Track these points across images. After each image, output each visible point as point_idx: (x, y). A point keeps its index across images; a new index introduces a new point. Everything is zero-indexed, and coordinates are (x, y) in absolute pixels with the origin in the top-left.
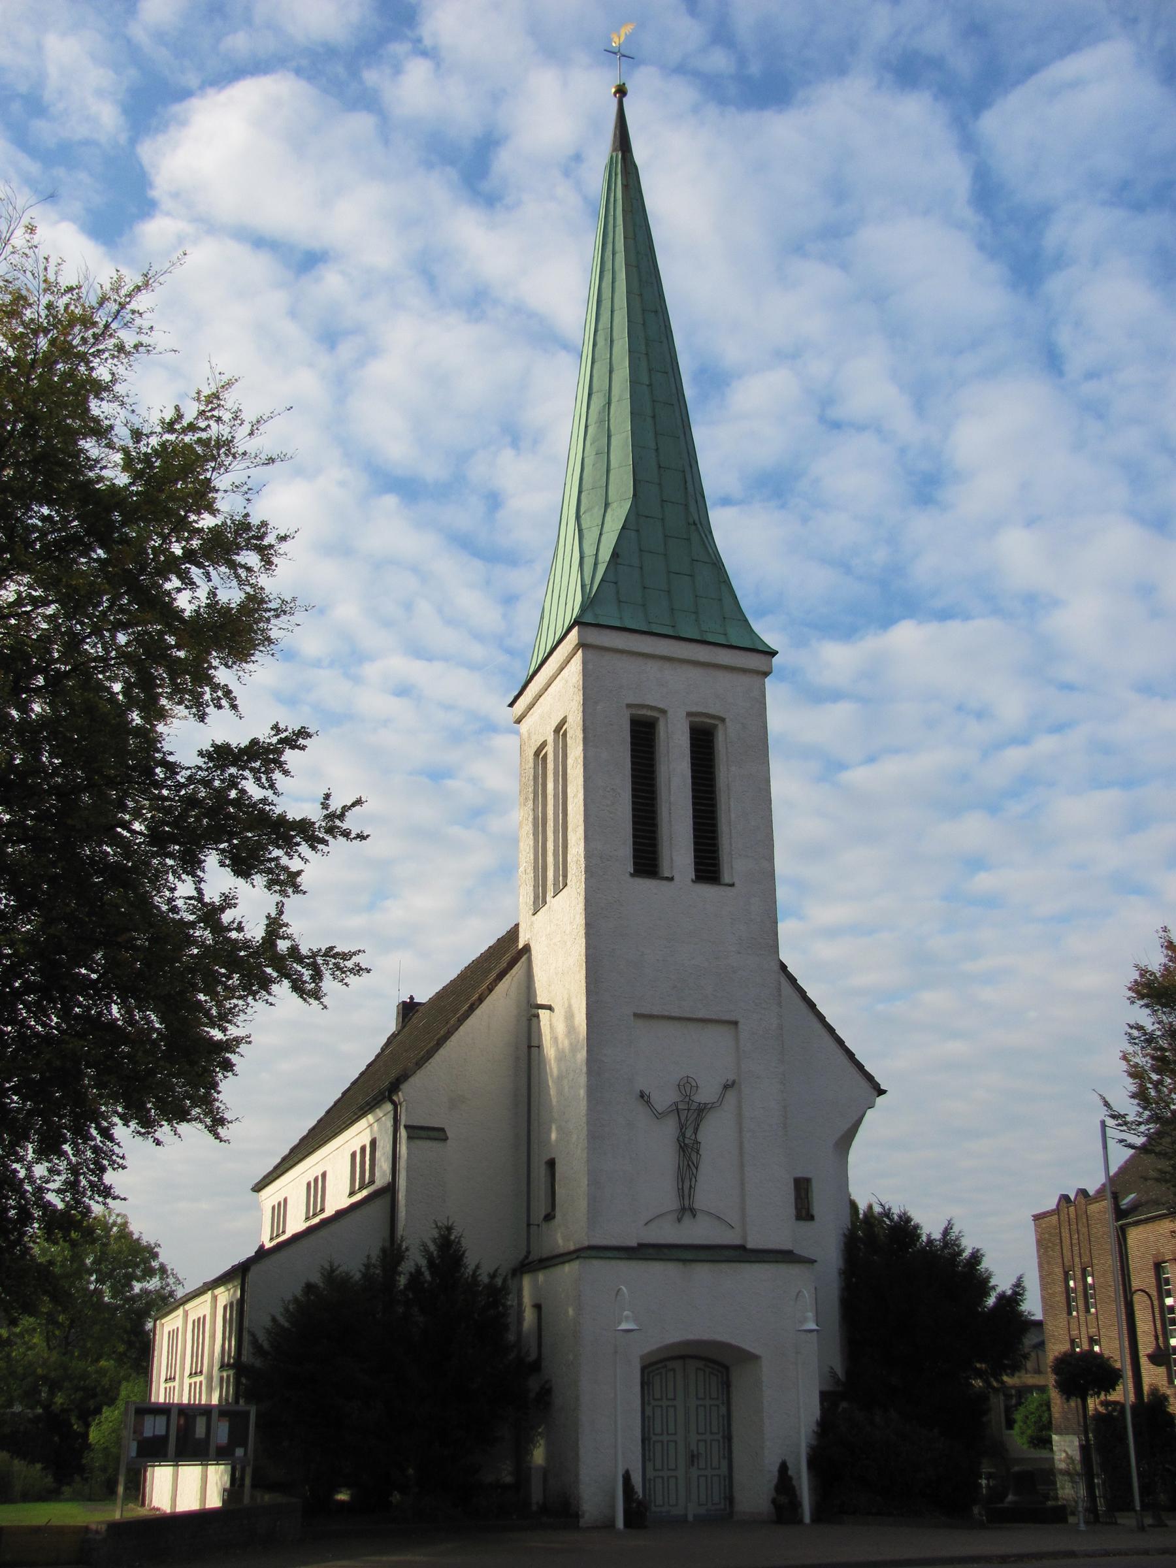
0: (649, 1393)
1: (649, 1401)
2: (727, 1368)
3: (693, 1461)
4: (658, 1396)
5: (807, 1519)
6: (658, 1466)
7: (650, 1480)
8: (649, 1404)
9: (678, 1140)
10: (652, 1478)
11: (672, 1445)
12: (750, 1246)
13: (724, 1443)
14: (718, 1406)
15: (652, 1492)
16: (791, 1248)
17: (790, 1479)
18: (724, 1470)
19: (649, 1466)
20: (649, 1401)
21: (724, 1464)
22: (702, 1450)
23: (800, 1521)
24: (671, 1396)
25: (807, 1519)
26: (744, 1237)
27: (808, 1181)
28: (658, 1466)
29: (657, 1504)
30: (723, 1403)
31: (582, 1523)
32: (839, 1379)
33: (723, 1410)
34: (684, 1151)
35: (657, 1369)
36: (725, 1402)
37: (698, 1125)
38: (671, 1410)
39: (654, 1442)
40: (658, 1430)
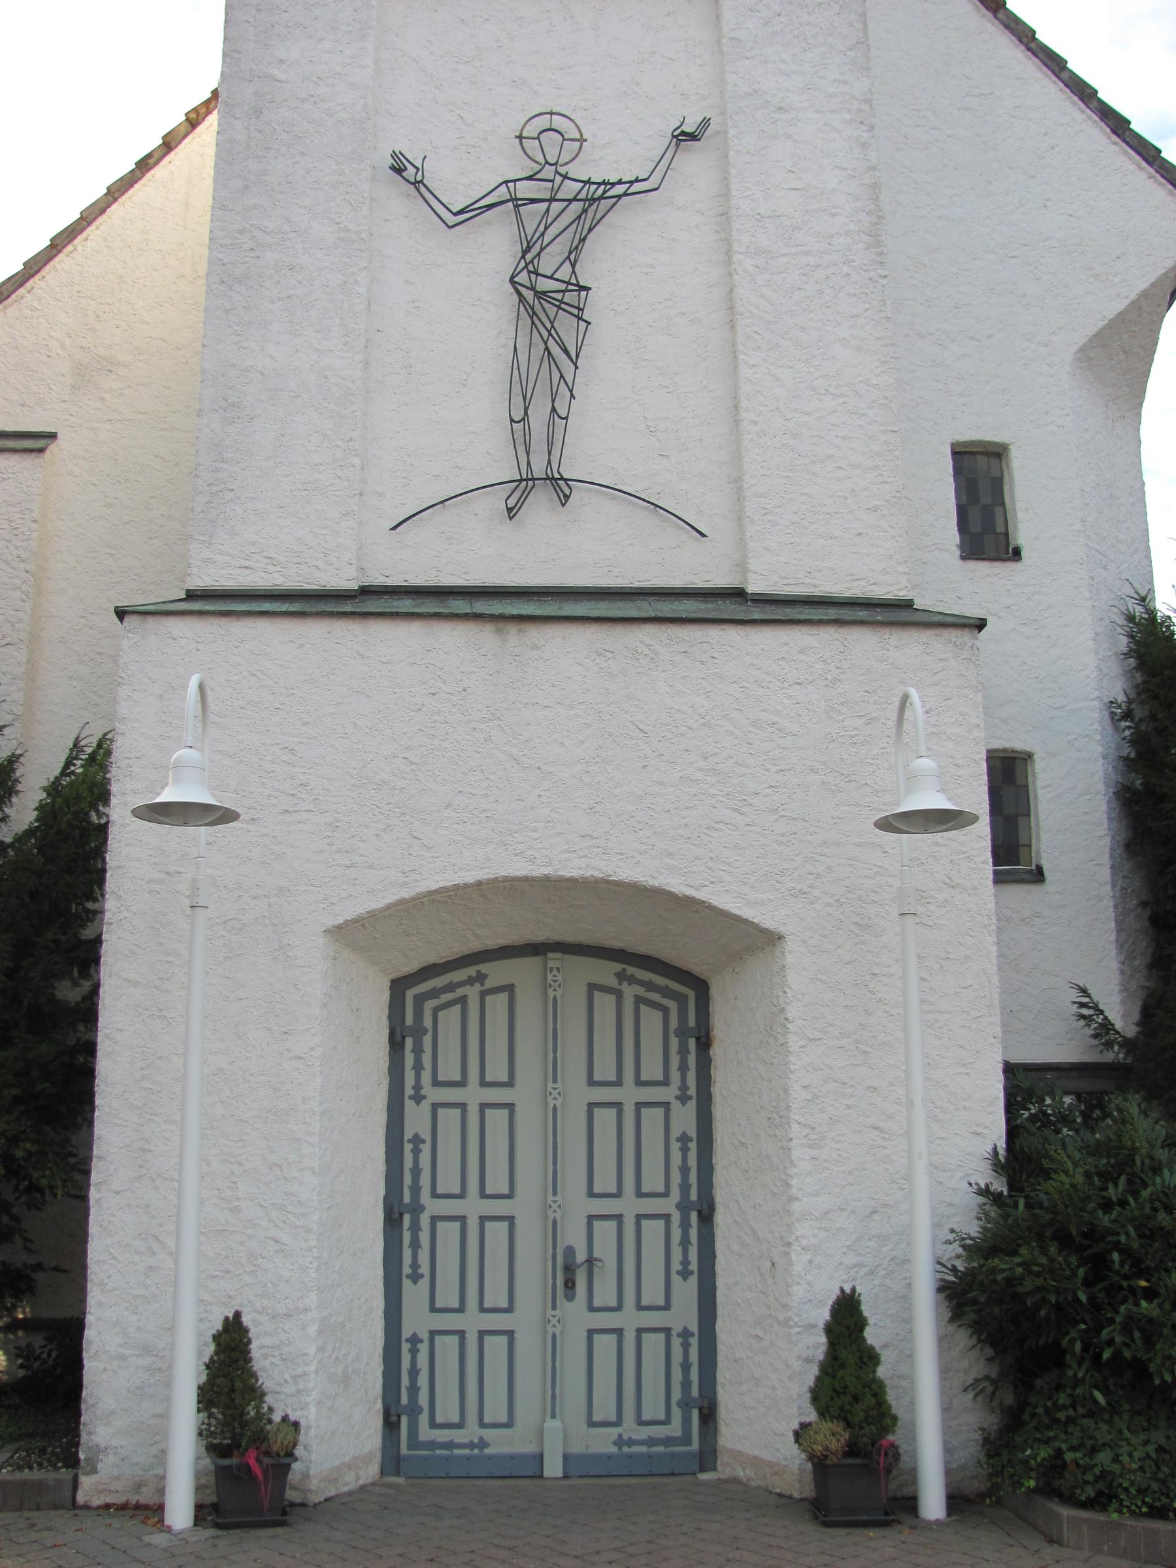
0: (418, 1067)
1: (418, 1087)
2: (701, 987)
3: (570, 1285)
4: (450, 1069)
5: (933, 1505)
6: (448, 1296)
7: (415, 1340)
8: (418, 1098)
9: (512, 280)
10: (424, 1336)
11: (497, 1232)
12: (751, 589)
13: (685, 1225)
14: (666, 1105)
15: (423, 1380)
16: (903, 594)
17: (870, 1358)
18: (685, 1314)
19: (414, 1296)
20: (418, 1087)
21: (686, 1292)
22: (605, 1249)
23: (910, 1504)
24: (497, 1070)
25: (933, 1505)
26: (742, 566)
27: (997, 453)
28: (448, 1296)
29: (439, 1419)
30: (683, 1099)
31: (90, 1489)
32: (1107, 1026)
33: (685, 1119)
34: (533, 314)
35: (451, 987)
36: (692, 1091)
37: (583, 240)
38: (497, 1120)
39: (434, 1220)
40: (449, 1181)
